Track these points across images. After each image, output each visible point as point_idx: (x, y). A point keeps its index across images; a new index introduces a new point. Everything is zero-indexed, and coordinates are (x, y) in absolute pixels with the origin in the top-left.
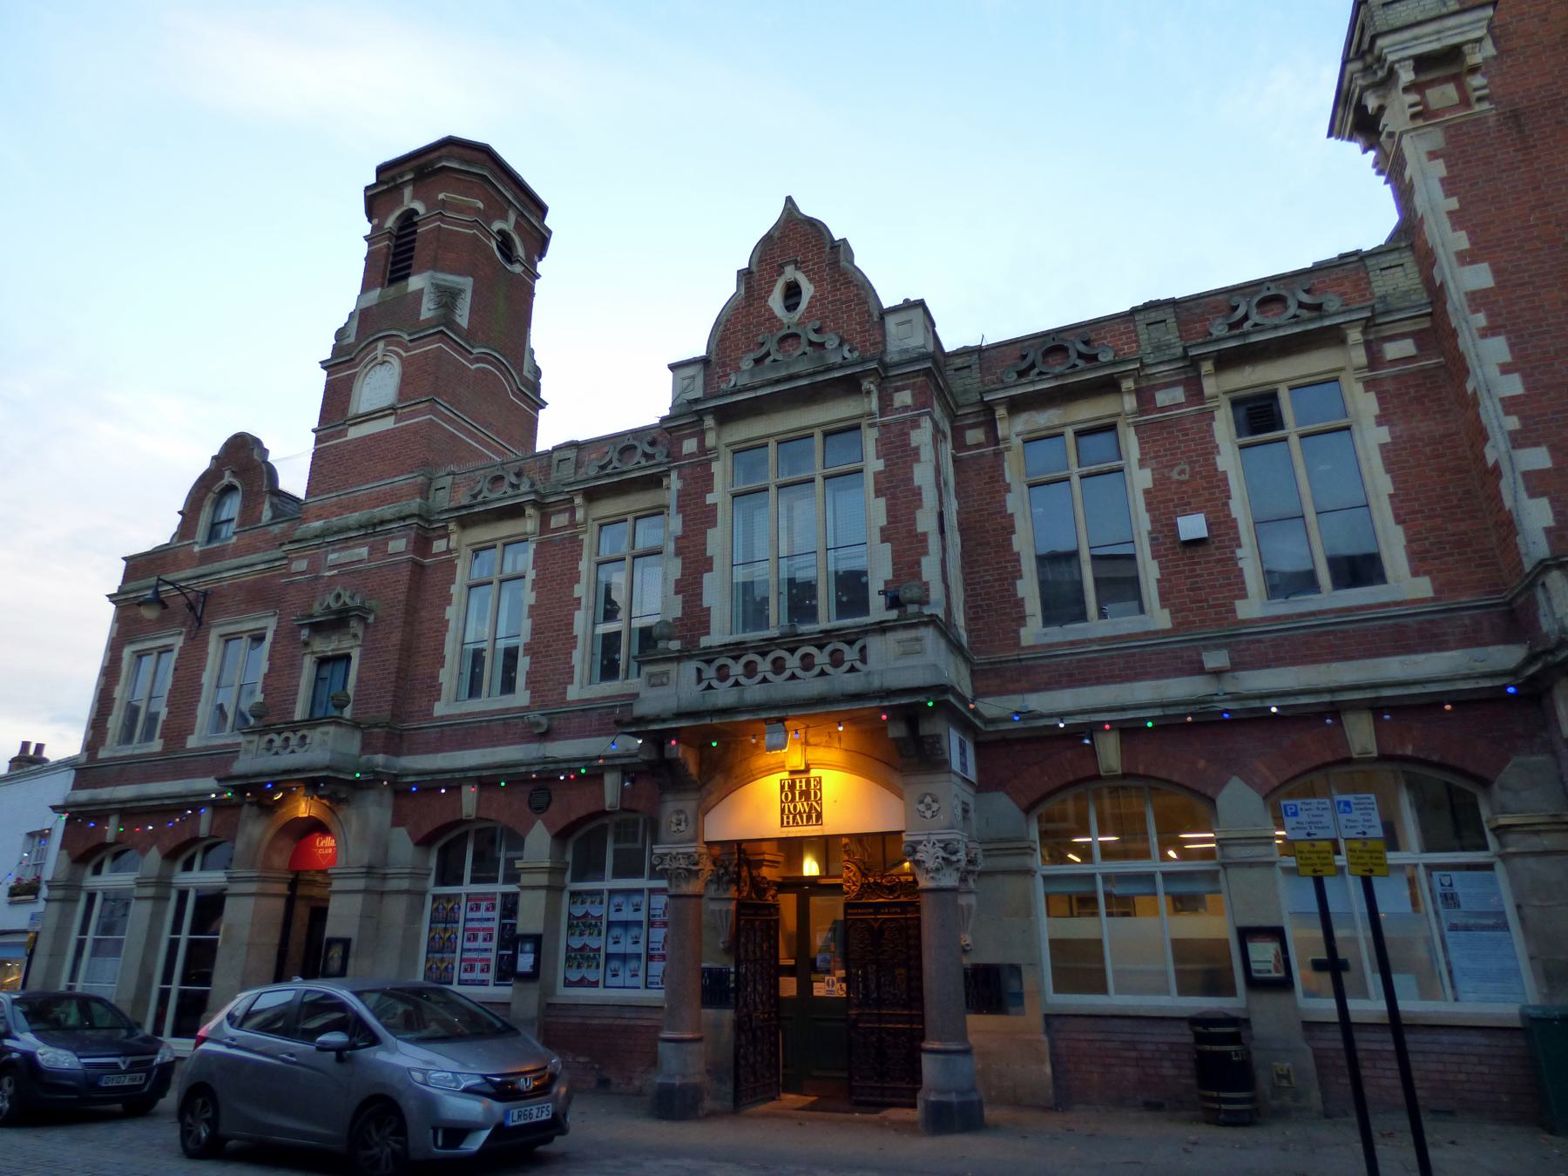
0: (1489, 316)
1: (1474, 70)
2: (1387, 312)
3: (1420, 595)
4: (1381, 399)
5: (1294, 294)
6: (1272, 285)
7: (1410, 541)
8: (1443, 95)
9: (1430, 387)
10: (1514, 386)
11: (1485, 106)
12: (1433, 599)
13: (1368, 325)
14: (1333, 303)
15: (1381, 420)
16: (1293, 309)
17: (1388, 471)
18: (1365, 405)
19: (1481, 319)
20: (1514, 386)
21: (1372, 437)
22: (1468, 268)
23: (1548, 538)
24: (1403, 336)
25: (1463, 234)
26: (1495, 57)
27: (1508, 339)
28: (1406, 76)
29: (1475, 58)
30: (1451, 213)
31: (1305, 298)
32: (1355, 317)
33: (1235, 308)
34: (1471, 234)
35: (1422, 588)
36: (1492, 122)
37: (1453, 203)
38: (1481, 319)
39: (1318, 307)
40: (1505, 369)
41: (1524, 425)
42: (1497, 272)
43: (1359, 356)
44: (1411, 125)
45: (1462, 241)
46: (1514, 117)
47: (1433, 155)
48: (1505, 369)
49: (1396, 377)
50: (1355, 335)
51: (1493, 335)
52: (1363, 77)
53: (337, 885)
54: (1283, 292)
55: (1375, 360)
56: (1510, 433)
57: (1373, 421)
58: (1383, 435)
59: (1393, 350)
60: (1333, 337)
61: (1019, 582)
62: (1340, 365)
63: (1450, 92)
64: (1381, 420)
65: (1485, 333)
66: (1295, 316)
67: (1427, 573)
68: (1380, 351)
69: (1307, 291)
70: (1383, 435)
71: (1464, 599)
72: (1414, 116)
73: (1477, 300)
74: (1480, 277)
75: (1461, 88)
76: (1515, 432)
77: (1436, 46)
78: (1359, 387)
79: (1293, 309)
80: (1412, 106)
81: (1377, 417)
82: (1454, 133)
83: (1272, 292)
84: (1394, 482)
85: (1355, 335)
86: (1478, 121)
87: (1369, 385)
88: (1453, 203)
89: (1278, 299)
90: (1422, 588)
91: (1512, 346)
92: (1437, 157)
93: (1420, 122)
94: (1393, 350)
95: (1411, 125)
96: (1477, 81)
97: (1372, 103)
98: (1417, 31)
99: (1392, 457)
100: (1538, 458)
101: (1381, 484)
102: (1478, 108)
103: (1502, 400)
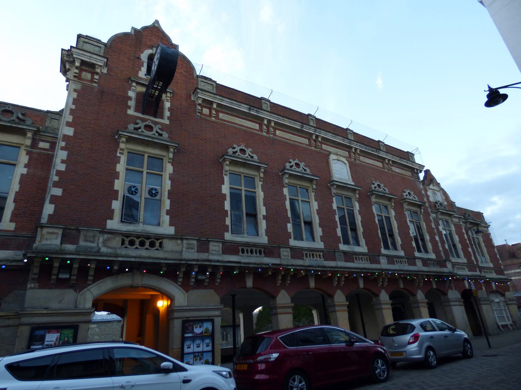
0: (66, 144)
1: (97, 74)
2: (45, 132)
3: (9, 229)
4: (30, 159)
5: (17, 113)
6: (11, 107)
7: (15, 209)
8: (87, 76)
9: (41, 161)
10: (62, 167)
11: (96, 85)
12: (13, 231)
13: (36, 133)
14: (29, 121)
15: (26, 166)
16: (154, 132)
17: (20, 183)
18: (24, 158)
19: (63, 144)
20: (62, 167)
21: (21, 170)
22: (68, 128)
23: (49, 218)
24: (48, 142)
25: (72, 117)
26: (105, 74)
27: (68, 153)
28: (77, 64)
29: (98, 71)
30: (71, 109)
31: (20, 116)
32: (31, 128)
33: (138, 124)
34: (74, 118)
35: (12, 226)
36: (96, 90)
37: (73, 107)
38: (63, 144)
39: (24, 121)
40: (63, 162)
41: (59, 180)
42: (75, 132)
43: (28, 142)
44: (73, 79)
45: (70, 119)
46: (102, 92)
47: (75, 90)
48: (63, 162)
49: (39, 154)
50: (29, 135)
51: (65, 150)
52: (67, 57)
53: (37, 276)
54: (13, 111)
55: (34, 144)
56: (54, 181)
57: (23, 165)
58: (25, 171)
59: (42, 145)
60: (22, 132)
61: (17, 190)
62: (22, 143)
63: (89, 76)
64: (26, 166)
65: (62, 149)
66: (14, 120)
67: (15, 222)
68: (38, 144)
69: (22, 114)
70: (25, 171)
71: (24, 233)
72: (75, 76)
73: (66, 138)
74: (70, 131)
75: (92, 77)
76: (56, 182)
77: (88, 60)
78: (24, 152)
79: (154, 132)
80: (75, 73)
81: (25, 164)
82: (84, 87)
83: (10, 109)
84: (20, 188)
85: (29, 135)
86: (92, 88)
87: (28, 153)
88: (73, 107)
89: (11, 112)
90: (12, 226)
91: (68, 155)
92: (76, 92)
93: (76, 79)
94: (42, 145)
95: (73, 79)
96: (96, 77)
97: (67, 66)
98: (84, 53)
99: (23, 179)
100: (58, 192)
101: (16, 187)
102: (94, 84)
103: (57, 170)
